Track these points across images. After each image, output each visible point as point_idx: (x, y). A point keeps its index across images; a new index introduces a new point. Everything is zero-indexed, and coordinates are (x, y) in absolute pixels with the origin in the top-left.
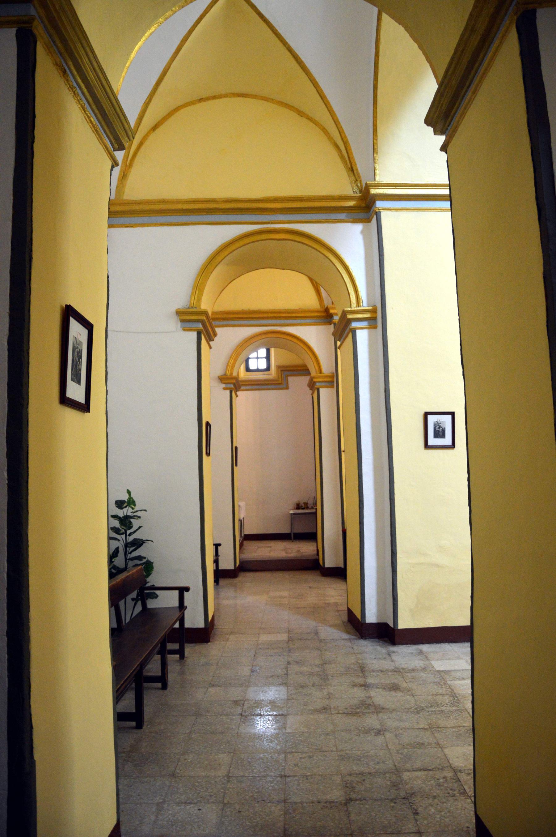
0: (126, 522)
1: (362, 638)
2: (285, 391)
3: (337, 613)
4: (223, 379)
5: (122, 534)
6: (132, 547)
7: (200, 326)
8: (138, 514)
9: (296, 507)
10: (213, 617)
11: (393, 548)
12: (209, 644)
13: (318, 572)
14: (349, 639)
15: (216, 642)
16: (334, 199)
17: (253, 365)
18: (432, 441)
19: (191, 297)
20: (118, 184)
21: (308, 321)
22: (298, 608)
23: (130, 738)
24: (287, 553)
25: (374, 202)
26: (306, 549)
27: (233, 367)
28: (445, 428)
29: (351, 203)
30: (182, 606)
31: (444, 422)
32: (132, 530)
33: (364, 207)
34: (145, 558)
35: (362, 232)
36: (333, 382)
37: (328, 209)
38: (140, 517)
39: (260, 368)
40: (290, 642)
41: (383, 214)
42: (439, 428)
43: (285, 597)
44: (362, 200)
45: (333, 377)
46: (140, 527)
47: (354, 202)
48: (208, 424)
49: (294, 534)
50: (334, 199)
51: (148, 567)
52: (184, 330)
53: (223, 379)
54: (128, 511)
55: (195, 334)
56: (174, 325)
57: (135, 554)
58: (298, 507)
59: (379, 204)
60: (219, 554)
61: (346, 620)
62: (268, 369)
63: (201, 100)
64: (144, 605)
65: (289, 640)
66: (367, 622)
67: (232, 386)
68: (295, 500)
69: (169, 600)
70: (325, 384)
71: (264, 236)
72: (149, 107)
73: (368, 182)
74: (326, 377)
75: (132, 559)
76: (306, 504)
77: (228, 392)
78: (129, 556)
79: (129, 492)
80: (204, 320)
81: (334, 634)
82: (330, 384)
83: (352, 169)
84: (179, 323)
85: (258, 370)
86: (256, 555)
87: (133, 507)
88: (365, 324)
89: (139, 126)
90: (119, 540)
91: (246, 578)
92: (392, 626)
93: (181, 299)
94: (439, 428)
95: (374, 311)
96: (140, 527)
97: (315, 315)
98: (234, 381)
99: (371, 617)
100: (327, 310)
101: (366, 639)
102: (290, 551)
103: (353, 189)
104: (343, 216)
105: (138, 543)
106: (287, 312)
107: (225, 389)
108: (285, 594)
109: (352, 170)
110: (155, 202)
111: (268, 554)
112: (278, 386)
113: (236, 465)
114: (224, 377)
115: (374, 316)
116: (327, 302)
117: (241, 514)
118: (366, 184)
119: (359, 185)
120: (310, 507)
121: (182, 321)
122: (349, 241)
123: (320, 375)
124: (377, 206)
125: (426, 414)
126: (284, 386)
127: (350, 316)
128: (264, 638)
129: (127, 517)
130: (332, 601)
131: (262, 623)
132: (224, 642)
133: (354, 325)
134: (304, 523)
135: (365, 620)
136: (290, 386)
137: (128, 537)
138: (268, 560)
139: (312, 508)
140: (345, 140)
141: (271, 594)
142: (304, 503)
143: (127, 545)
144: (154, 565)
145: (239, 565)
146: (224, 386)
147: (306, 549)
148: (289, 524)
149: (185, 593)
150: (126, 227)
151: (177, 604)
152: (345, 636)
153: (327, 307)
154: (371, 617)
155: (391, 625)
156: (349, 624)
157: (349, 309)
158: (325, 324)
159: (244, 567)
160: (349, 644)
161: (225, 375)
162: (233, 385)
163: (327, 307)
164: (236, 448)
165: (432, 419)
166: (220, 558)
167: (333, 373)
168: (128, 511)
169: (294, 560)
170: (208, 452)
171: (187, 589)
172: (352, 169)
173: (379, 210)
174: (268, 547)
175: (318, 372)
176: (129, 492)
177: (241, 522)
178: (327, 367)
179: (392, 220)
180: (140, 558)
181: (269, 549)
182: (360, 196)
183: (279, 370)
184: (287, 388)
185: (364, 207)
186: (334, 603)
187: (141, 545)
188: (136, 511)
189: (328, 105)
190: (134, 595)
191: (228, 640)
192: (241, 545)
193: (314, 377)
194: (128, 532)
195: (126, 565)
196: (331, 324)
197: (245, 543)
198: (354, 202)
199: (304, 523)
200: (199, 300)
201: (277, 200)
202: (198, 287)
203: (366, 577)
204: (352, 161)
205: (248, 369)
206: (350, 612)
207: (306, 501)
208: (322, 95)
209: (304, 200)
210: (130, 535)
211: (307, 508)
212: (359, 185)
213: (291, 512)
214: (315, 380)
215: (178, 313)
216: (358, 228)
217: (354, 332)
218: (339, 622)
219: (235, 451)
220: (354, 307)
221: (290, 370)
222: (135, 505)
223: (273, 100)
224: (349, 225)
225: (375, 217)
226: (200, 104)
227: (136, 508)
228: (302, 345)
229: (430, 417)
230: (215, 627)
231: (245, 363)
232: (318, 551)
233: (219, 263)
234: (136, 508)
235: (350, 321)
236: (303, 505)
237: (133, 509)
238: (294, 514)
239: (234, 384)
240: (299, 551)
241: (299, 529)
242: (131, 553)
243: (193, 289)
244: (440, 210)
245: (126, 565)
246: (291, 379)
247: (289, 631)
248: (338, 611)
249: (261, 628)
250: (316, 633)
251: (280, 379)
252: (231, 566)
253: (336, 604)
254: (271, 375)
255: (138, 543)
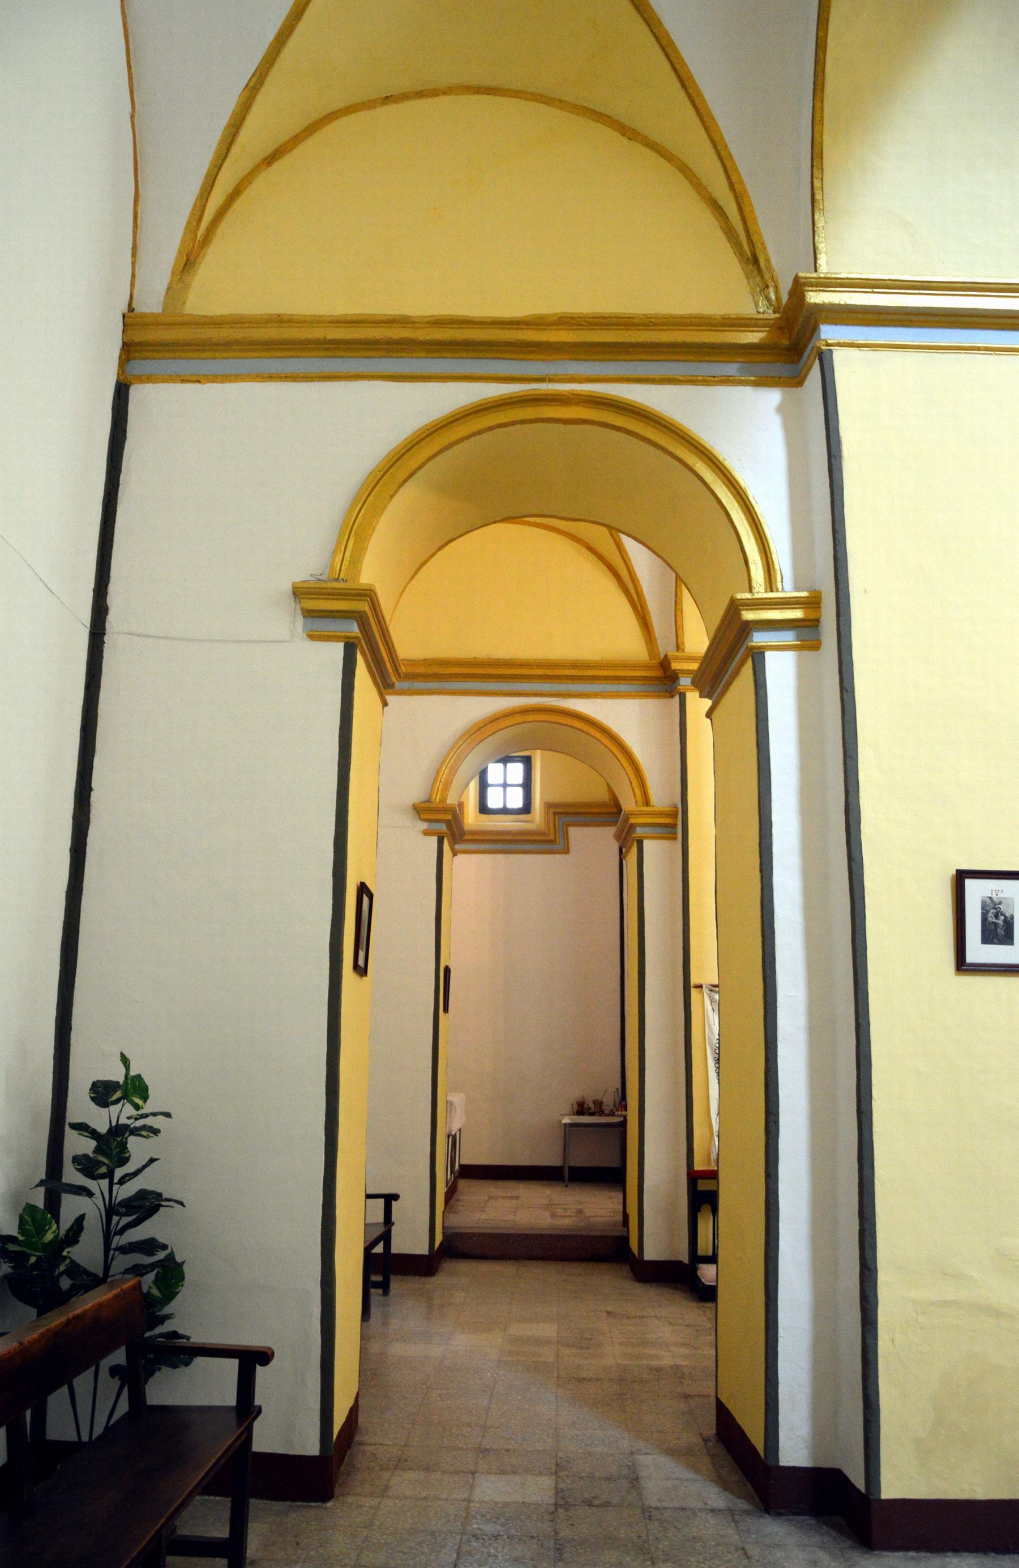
0: (113, 1144)
1: (768, 1513)
2: (558, 857)
3: (683, 1406)
4: (423, 811)
5: (102, 1176)
6: (127, 1215)
7: (354, 629)
8: (149, 1121)
9: (576, 1108)
10: (354, 1411)
11: (868, 1256)
12: (329, 1504)
13: (626, 1268)
14: (731, 1511)
15: (350, 1499)
16: (710, 325)
17: (494, 801)
18: (977, 951)
19: (334, 552)
20: (171, 282)
21: (623, 687)
22: (581, 1380)
23: (365, 1324)
24: (553, 1216)
25: (815, 329)
26: (594, 1208)
27: (447, 785)
28: (1012, 917)
29: (754, 337)
30: (246, 1408)
31: (1011, 902)
32: (129, 1168)
33: (790, 346)
34: (164, 1247)
35: (781, 409)
36: (675, 826)
37: (696, 350)
38: (156, 1132)
39: (509, 806)
40: (561, 1511)
41: (841, 358)
42: (996, 916)
43: (548, 1342)
44: (780, 328)
45: (676, 816)
46: (152, 1160)
47: (761, 335)
48: (363, 890)
49: (569, 1167)
50: (710, 325)
51: (171, 1274)
52: (312, 637)
53: (423, 811)
54: (123, 1112)
55: (337, 649)
56: (285, 623)
57: (136, 1235)
58: (581, 1109)
59: (828, 333)
60: (394, 1218)
61: (711, 1432)
62: (527, 808)
63: (387, 100)
64: (137, 1397)
65: (556, 1505)
66: (781, 1464)
67: (443, 827)
68: (576, 1094)
69: (211, 1385)
70: (659, 830)
71: (530, 412)
72: (259, 98)
73: (801, 274)
74: (660, 814)
75: (124, 1250)
76: (599, 1104)
77: (434, 840)
78: (117, 1241)
79: (125, 1060)
80: (365, 612)
81: (682, 1486)
82: (670, 830)
83: (753, 260)
84: (300, 621)
85: (505, 811)
86: (484, 1216)
87: (140, 1102)
88: (788, 637)
89: (231, 144)
90: (90, 1194)
91: (459, 1278)
92: (863, 1490)
93: (308, 559)
94: (996, 916)
95: (813, 603)
96: (152, 1160)
97: (638, 673)
98: (450, 817)
99: (794, 1449)
100: (665, 664)
101: (779, 1515)
102: (560, 1212)
103: (757, 306)
104: (731, 369)
105: (147, 1204)
106: (575, 665)
107: (426, 833)
108: (548, 1330)
109: (756, 261)
110: (256, 322)
111: (511, 1217)
112: (547, 847)
113: (446, 1010)
114: (428, 805)
115: (812, 615)
116: (665, 646)
117: (453, 1121)
118: (796, 279)
119: (773, 296)
120: (607, 1112)
121: (309, 614)
122: (749, 430)
123: (645, 808)
124: (823, 336)
125: (961, 877)
126: (560, 846)
127: (749, 615)
128: (491, 1489)
129: (119, 1131)
130: (667, 1360)
131: (485, 1428)
132: (375, 1502)
133: (759, 639)
134: (596, 1147)
135: (778, 1459)
136: (572, 849)
137: (115, 1187)
138: (510, 1235)
139: (612, 1114)
140: (737, 187)
141: (517, 1329)
142: (594, 1102)
143: (111, 1210)
144: (185, 1267)
145: (441, 1243)
146: (425, 826)
147: (594, 1208)
148: (558, 1147)
149: (258, 1368)
150: (183, 381)
151: (231, 1399)
152: (715, 1497)
153: (666, 656)
154: (794, 1449)
155: (859, 1482)
156: (721, 1451)
157: (748, 596)
158: (658, 697)
159: (456, 1248)
160: (731, 1534)
161: (429, 801)
162: (446, 827)
163: (666, 656)
164: (447, 970)
165: (976, 891)
166: (394, 1230)
167: (675, 806)
168: (123, 1112)
169: (574, 1237)
170: (361, 963)
171: (264, 1357)
172: (753, 260)
173: (828, 345)
174: (512, 1198)
175: (640, 803)
176: (125, 1060)
177: (453, 1140)
178: (661, 793)
179: (863, 373)
180: (150, 1246)
181: (514, 1202)
182: (776, 319)
183: (551, 814)
184: (566, 851)
185: (790, 346)
186: (672, 1367)
187: (154, 1209)
188: (146, 1116)
189: (697, 100)
190: (119, 1357)
191: (384, 1492)
192: (451, 1192)
193: (633, 814)
194: (119, 1173)
195: (107, 1267)
196: (672, 697)
197: (462, 1184)
198: (761, 335)
199: (596, 1147)
200: (356, 562)
201: (565, 323)
202: (354, 528)
203: (781, 1333)
204: (755, 238)
205: (483, 808)
206: (723, 1413)
207: (598, 1097)
208: (684, 77)
209: (634, 324)
210: (122, 1181)
211: (601, 1113)
212: (773, 296)
213: (566, 1120)
214: (632, 821)
215: (299, 593)
216: (772, 397)
217: (758, 657)
218: (690, 1438)
219: (443, 978)
220: (760, 591)
221: (577, 814)
222: (145, 1098)
223: (561, 101)
224: (748, 390)
225: (817, 362)
226: (384, 108)
227: (148, 1108)
228: (606, 741)
229: (970, 884)
230: (357, 1438)
231: (478, 776)
232: (626, 1216)
233: (411, 476)
234: (148, 1108)
235: (748, 628)
236: (592, 1106)
237: (137, 1107)
238: (571, 1125)
239: (448, 823)
240: (580, 1211)
241: (580, 1159)
242: (121, 1232)
243: (341, 534)
244: (987, 349)
245: (107, 1267)
246: (574, 832)
247: (559, 1469)
248: (686, 1397)
249: (483, 1451)
250: (635, 1481)
251: (552, 832)
252: (421, 1248)
253: (678, 1373)
254: (532, 822)
255: (147, 1204)
